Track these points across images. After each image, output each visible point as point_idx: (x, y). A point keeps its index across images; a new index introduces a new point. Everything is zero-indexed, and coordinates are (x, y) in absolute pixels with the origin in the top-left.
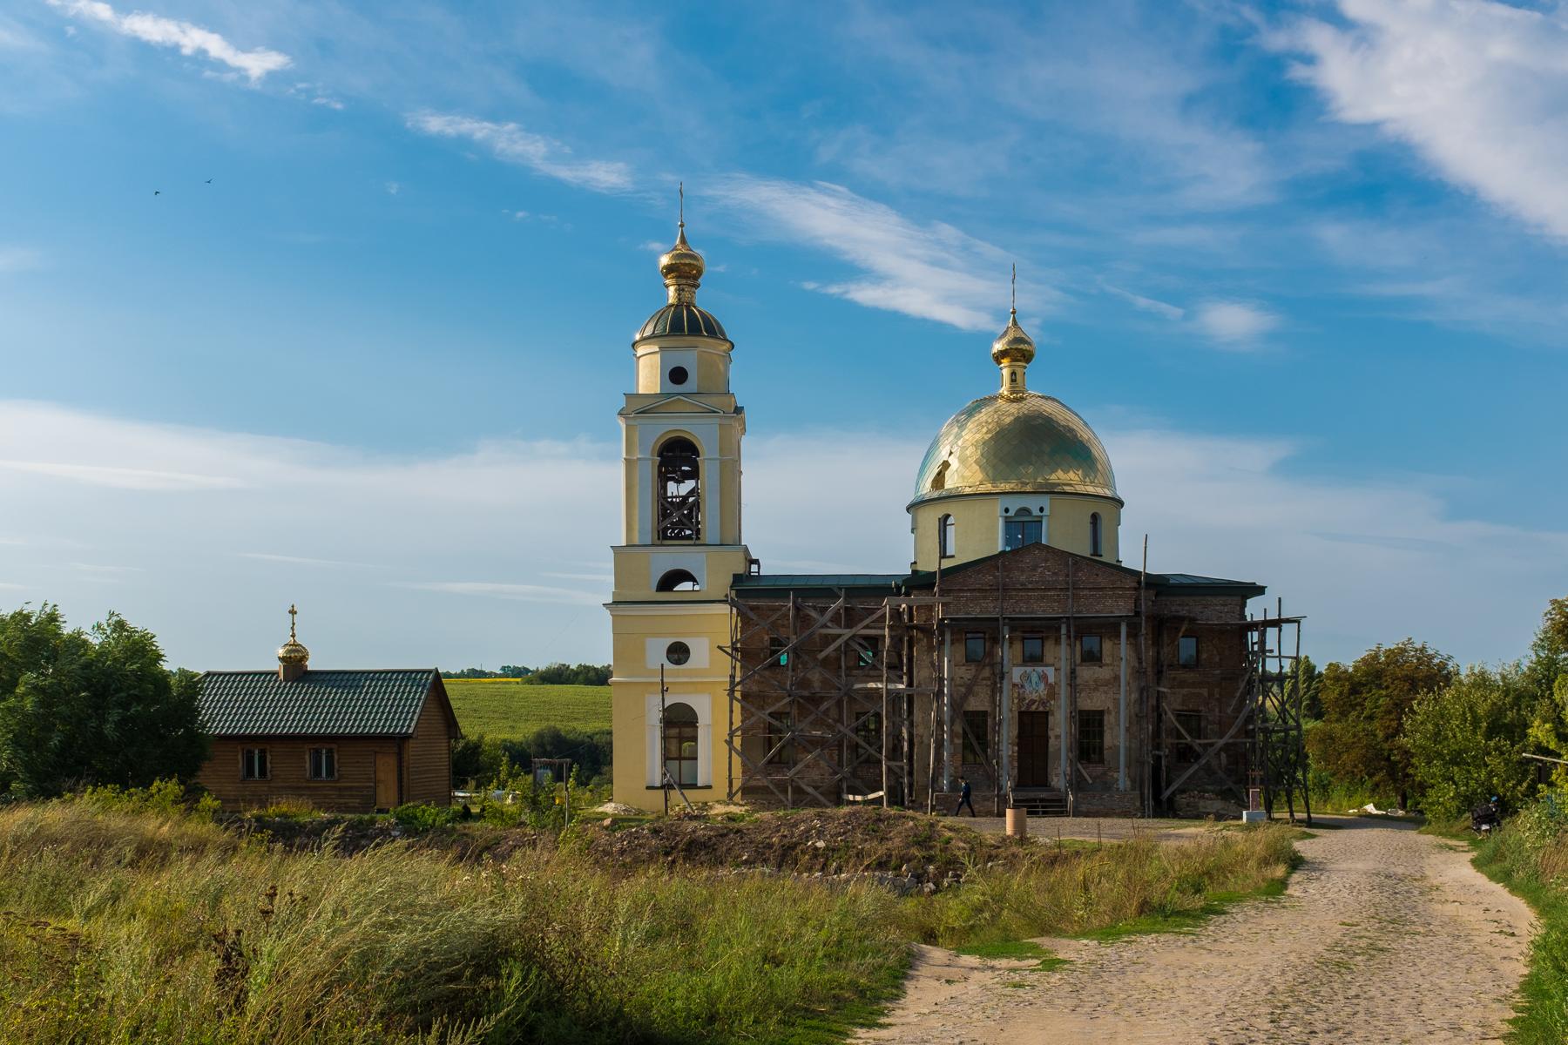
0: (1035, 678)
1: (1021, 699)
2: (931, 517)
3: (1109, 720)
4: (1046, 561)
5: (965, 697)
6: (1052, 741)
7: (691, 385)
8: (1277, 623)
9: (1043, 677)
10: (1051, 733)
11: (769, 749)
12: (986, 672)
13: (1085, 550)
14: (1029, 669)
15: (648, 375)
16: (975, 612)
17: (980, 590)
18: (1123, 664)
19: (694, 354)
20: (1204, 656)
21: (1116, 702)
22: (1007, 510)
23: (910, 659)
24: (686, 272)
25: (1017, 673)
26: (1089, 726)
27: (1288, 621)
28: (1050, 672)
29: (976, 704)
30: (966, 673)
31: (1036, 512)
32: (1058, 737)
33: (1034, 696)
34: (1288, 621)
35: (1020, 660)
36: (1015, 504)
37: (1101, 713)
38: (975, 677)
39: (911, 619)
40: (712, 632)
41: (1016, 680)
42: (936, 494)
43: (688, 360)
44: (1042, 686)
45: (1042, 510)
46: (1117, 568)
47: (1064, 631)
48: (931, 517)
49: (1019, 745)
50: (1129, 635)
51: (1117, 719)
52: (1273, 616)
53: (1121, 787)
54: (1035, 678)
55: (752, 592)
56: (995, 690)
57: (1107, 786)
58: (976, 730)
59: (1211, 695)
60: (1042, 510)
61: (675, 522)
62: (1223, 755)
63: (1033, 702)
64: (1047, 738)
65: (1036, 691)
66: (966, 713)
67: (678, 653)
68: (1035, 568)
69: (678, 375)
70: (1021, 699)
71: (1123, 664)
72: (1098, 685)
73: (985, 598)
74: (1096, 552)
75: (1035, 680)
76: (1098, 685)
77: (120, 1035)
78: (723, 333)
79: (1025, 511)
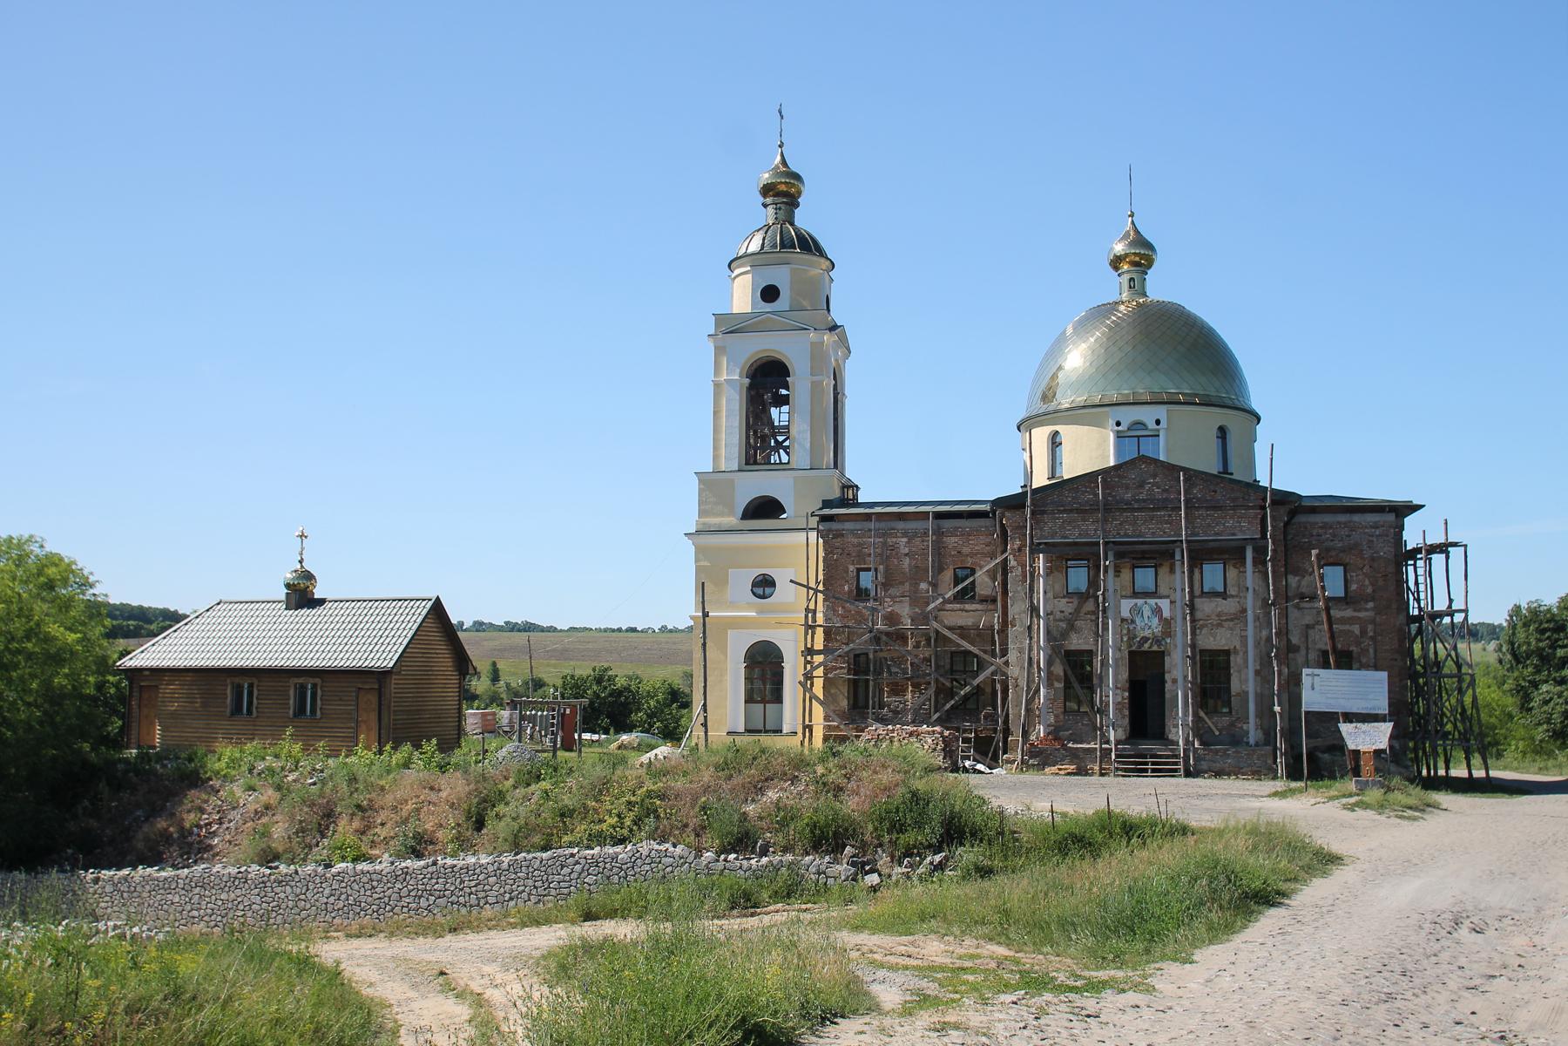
0: (1147, 612)
1: (1132, 637)
2: (1041, 435)
3: (1235, 660)
5: (1065, 635)
6: (1168, 686)
7: (782, 303)
8: (1443, 548)
9: (1157, 611)
10: (1167, 676)
13: (1211, 465)
15: (741, 296)
16: (1073, 536)
17: (1078, 511)
18: (1250, 595)
19: (785, 269)
20: (1354, 587)
21: (1244, 639)
22: (1118, 424)
23: (250, 703)
24: (783, 192)
26: (1213, 672)
27: (1455, 545)
28: (1164, 604)
29: (1076, 642)
31: (1152, 425)
32: (1175, 681)
33: (1147, 633)
34: (1455, 545)
35: (1129, 592)
36: (1129, 415)
37: (1227, 653)
38: (1077, 610)
40: (796, 554)
41: (1125, 613)
42: (1043, 408)
44: (1155, 621)
45: (1158, 422)
46: (1255, 485)
47: (1178, 557)
48: (1041, 435)
50: (1255, 563)
52: (1436, 538)
53: (1252, 741)
54: (1147, 612)
55: (841, 514)
57: (1236, 740)
58: (1077, 673)
59: (1363, 632)
60: (1158, 422)
61: (761, 442)
63: (1145, 639)
64: (1163, 682)
65: (1148, 625)
66: (1068, 653)
67: (764, 585)
68: (1141, 486)
69: (770, 294)
70: (1132, 637)
71: (1250, 595)
72: (1221, 621)
73: (1084, 520)
74: (1225, 471)
75: (1145, 609)
76: (1221, 621)
79: (1139, 424)
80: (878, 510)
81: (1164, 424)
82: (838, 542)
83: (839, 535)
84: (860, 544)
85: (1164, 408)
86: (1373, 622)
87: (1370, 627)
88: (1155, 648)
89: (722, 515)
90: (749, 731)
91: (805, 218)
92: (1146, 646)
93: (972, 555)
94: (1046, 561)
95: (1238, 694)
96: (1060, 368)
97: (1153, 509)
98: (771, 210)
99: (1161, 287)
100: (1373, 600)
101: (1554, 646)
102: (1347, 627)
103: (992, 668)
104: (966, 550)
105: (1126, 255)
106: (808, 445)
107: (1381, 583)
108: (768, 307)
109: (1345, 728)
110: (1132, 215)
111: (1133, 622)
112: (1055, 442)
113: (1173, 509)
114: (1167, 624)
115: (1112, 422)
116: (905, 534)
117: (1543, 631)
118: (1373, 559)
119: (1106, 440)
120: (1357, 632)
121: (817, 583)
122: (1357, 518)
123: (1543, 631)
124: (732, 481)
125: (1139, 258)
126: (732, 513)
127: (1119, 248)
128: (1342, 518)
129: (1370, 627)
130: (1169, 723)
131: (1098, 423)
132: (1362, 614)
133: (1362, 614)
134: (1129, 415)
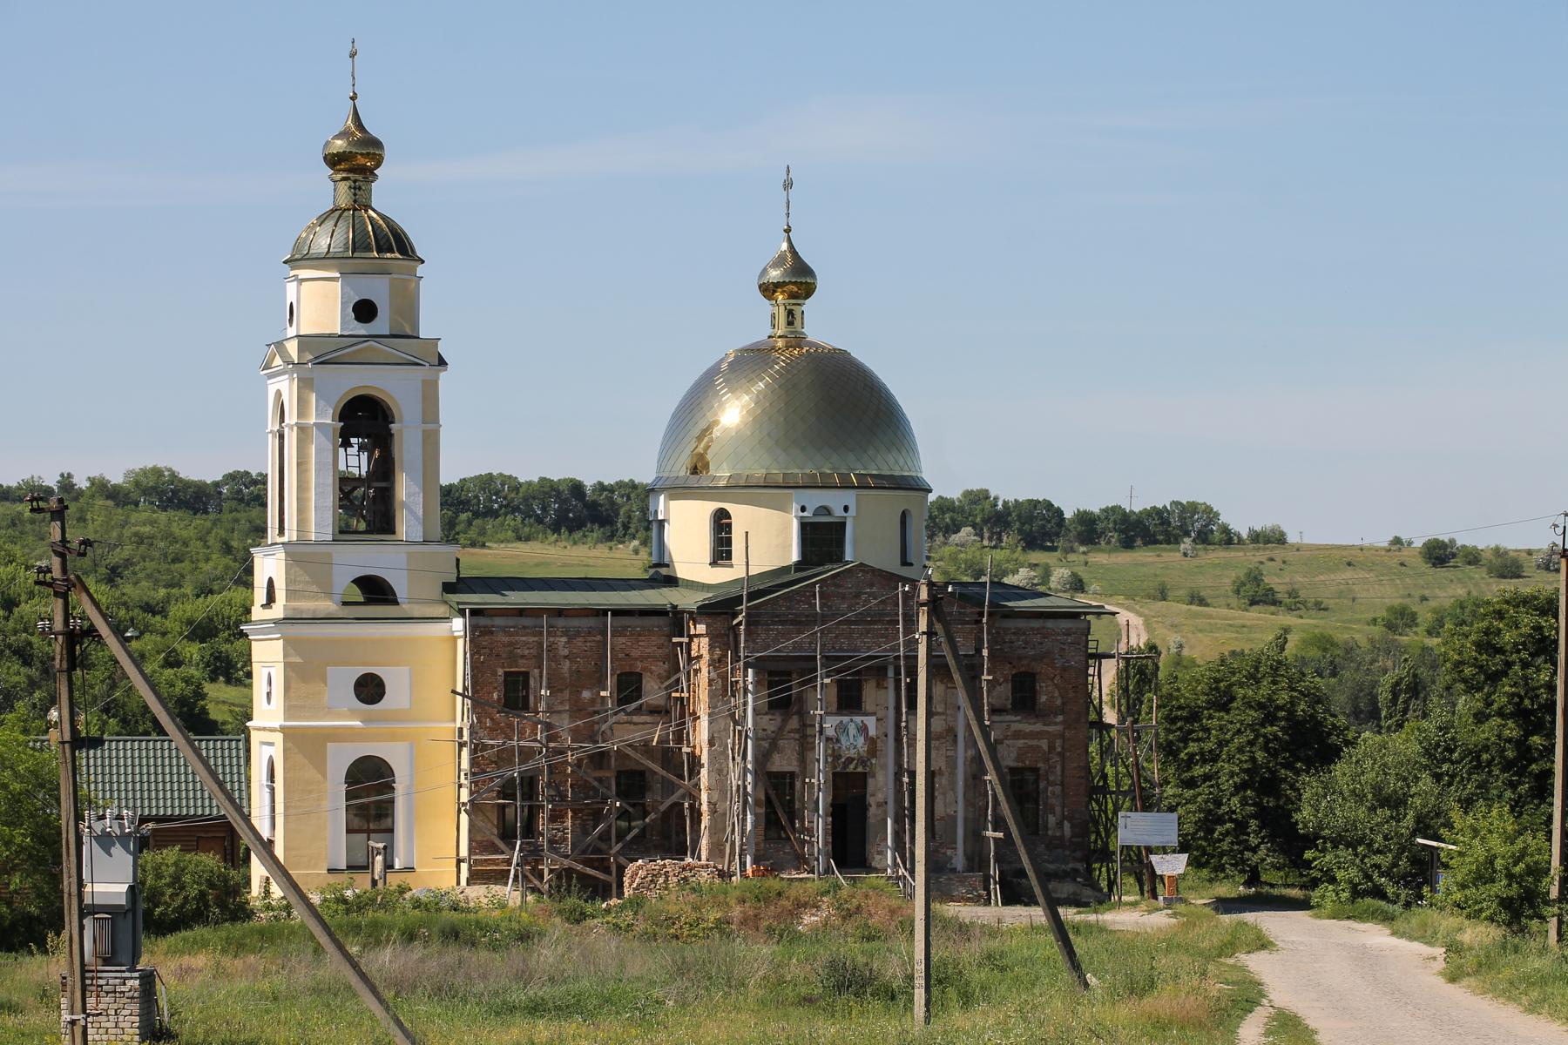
0: (852, 730)
1: (836, 756)
4: (871, 585)
7: (381, 325)
9: (863, 729)
10: (871, 800)
11: (507, 817)
12: (794, 723)
14: (846, 719)
17: (793, 622)
22: (803, 509)
24: (357, 161)
25: (830, 724)
28: (871, 722)
29: (782, 763)
30: (771, 723)
33: (852, 753)
35: (834, 707)
38: (781, 729)
39: (1118, 785)
41: (830, 732)
43: (377, 289)
44: (861, 740)
45: (846, 509)
49: (832, 815)
51: (953, 784)
53: (960, 868)
54: (852, 730)
56: (805, 746)
59: (1052, 748)
60: (846, 509)
62: (1067, 824)
65: (854, 744)
68: (857, 596)
69: (364, 311)
70: (836, 756)
77: (1565, 967)
78: (413, 251)
80: (515, 598)
81: (852, 512)
82: (485, 641)
83: (487, 631)
84: (511, 644)
85: (852, 493)
86: (1062, 736)
87: (1058, 743)
88: (860, 769)
89: (314, 596)
90: (349, 867)
91: (391, 195)
92: (852, 766)
93: (642, 658)
94: (756, 674)
95: (942, 818)
96: (716, 423)
97: (870, 623)
98: (343, 186)
99: (824, 324)
100: (1063, 712)
101: (1185, 740)
102: (1035, 742)
103: (681, 791)
104: (635, 653)
105: (784, 284)
106: (420, 513)
107: (1071, 695)
108: (362, 329)
109: (1154, 858)
110: (788, 231)
111: (838, 741)
112: (721, 523)
113: (889, 622)
114: (872, 743)
115: (795, 507)
116: (565, 633)
117: (1173, 721)
118: (1064, 669)
119: (788, 527)
120: (1045, 748)
121: (465, 688)
122: (1050, 624)
123: (1173, 721)
124: (330, 555)
125: (796, 283)
126: (328, 594)
127: (775, 275)
128: (1036, 624)
129: (1058, 743)
130: (871, 849)
131: (782, 507)
132: (1050, 729)
133: (1050, 729)
134: (816, 499)
